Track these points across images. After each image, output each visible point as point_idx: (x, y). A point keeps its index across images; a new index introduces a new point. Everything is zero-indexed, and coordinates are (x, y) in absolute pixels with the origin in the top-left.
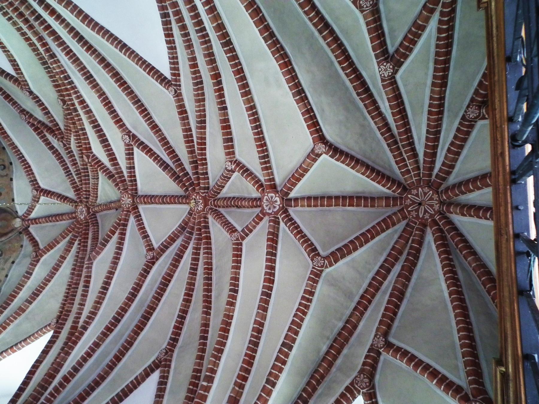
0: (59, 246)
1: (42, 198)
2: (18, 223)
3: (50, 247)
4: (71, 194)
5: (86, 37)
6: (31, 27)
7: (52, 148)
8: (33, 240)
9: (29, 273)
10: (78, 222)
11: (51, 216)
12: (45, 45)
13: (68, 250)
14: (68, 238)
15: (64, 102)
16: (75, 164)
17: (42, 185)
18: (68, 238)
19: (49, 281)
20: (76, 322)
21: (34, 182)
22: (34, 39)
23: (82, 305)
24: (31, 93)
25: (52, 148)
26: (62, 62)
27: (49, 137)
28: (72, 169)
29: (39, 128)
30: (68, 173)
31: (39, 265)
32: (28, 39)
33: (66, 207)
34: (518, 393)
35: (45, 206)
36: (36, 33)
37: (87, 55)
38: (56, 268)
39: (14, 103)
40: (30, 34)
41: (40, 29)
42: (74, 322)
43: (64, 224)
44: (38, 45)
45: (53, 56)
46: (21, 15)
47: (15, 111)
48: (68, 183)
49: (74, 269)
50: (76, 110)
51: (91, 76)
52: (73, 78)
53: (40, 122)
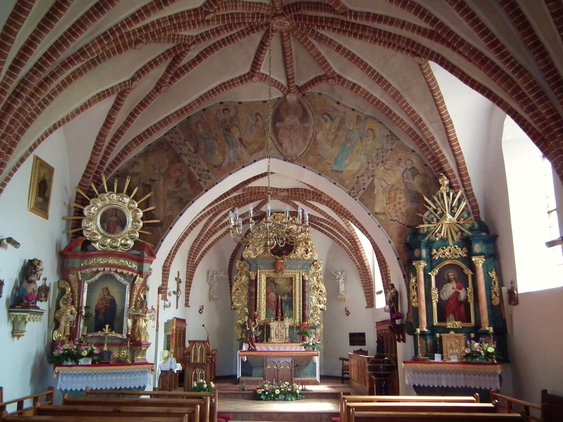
0: (323, 53)
1: (262, 71)
3: (323, 63)
4: (257, 37)
8: (312, 83)
9: (354, 87)
10: (294, 29)
12: (70, 61)
15: (137, 42)
16: (217, 31)
17: (247, 70)
18: (315, 42)
21: (243, 79)
22: (68, 73)
23: (403, 24)
24: (133, 79)
26: (87, 41)
27: (185, 61)
28: (225, 35)
29: (175, 72)
31: (344, 76)
33: (274, 42)
35: (272, 66)
38: (352, 57)
40: (62, 77)
43: (295, 47)
46: (41, 85)
47: (158, 97)
48: (243, 40)
50: (146, 27)
53: (168, 71)
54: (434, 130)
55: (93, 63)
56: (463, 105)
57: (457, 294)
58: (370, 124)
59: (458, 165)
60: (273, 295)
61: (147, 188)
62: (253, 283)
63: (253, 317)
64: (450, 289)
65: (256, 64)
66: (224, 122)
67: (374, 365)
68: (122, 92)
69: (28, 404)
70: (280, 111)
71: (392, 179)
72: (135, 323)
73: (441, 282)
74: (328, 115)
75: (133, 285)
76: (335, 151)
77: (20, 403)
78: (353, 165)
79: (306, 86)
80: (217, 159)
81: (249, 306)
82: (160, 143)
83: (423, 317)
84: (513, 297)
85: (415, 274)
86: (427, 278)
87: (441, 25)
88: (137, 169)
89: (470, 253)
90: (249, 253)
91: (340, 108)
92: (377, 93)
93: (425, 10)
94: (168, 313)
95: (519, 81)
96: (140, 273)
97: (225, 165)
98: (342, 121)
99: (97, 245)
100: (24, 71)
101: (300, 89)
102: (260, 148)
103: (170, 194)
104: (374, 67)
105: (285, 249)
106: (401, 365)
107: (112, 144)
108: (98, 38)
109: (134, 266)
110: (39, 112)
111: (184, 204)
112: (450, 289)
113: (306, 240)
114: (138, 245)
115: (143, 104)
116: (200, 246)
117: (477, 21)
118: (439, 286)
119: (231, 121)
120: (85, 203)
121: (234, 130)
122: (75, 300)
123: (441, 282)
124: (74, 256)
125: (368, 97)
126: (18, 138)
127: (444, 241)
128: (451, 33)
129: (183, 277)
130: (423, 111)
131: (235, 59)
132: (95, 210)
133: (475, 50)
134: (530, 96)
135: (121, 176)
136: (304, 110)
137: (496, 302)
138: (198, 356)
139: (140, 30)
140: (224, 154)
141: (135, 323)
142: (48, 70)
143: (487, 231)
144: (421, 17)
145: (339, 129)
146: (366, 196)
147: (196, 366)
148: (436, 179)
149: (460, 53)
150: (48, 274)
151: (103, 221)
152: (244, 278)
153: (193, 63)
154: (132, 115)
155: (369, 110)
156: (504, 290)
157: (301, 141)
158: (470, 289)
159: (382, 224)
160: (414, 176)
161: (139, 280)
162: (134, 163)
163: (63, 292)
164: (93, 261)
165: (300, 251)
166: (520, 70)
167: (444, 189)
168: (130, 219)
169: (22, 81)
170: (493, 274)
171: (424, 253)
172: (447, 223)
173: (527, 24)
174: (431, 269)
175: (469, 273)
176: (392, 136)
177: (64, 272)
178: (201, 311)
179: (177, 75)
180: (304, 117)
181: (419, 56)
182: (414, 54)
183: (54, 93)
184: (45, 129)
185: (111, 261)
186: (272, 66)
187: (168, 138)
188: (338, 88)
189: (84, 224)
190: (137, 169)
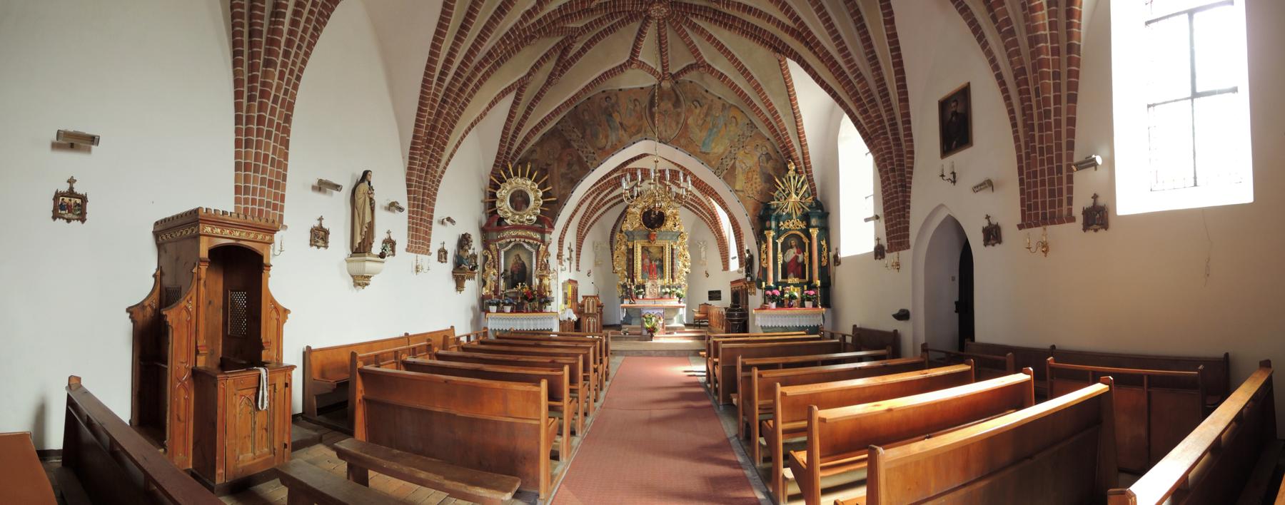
0: (695, 42)
1: (640, 58)
2: (666, 85)
3: (695, 52)
4: (635, 26)
5: (463, 15)
6: (469, 79)
7: (584, 50)
8: (685, 71)
9: (721, 76)
10: (670, 17)
11: (661, 48)
12: (481, 64)
13: (702, 32)
14: (688, 31)
15: (532, 37)
16: (600, 21)
17: (626, 58)
18: (688, 31)
19: (733, 56)
20: (786, 29)
21: (622, 68)
22: (479, 75)
23: (769, 18)
24: (529, 74)
25: (584, 50)
26: (493, 43)
27: (571, 54)
28: (607, 25)
29: (563, 65)
30: (611, 29)
31: (713, 65)
32: (480, 82)
33: (651, 32)
34: (180, 222)
35: (648, 54)
36: (473, 75)
37: (478, 16)
38: (721, 47)
39: (542, 91)
40: (475, 81)
41: (468, 72)
42: (787, 31)
43: (670, 34)
44: (484, 71)
45: (489, 54)
46: (461, 90)
47: (550, 91)
48: (623, 30)
49: (726, 25)
50: (539, 21)
51: (499, 8)
52: (507, 29)
53: (557, 64)
54: (787, 122)
55: (498, 64)
56: (811, 99)
57: (797, 257)
58: (733, 113)
59: (803, 154)
60: (647, 261)
61: (544, 172)
62: (631, 252)
63: (631, 276)
64: (792, 253)
65: (635, 52)
66: (607, 108)
67: (730, 312)
68: (520, 87)
69: (472, 339)
70: (653, 98)
71: (750, 161)
72: (541, 281)
73: (785, 247)
74: (697, 101)
75: (538, 252)
76: (704, 134)
77: (468, 337)
78: (718, 148)
79: (678, 74)
80: (602, 141)
81: (628, 270)
82: (553, 132)
83: (771, 275)
84: (837, 261)
85: (766, 241)
86: (775, 244)
87: (802, 24)
88: (535, 156)
89: (809, 226)
90: (627, 226)
91: (710, 97)
92: (741, 83)
93: (790, 8)
94: (564, 276)
95: (858, 87)
96: (543, 241)
97: (608, 147)
98: (710, 108)
99: (508, 221)
100: (448, 79)
101: (673, 77)
102: (638, 132)
103: (563, 176)
104: (740, 59)
105: (654, 220)
106: (752, 311)
107: (514, 137)
108: (502, 39)
109: (538, 236)
110: (460, 114)
111: (574, 182)
112: (792, 253)
113: (675, 215)
114: (539, 220)
115: (538, 98)
116: (587, 221)
117: (832, 25)
118: (784, 251)
119: (613, 106)
120: (497, 187)
121: (615, 115)
122: (496, 265)
123: (785, 247)
124: (493, 230)
125: (733, 86)
126: (447, 138)
127: (789, 216)
128: (810, 33)
129: (574, 247)
130: (779, 104)
131: (615, 49)
132: (504, 193)
133: (828, 52)
134: (865, 101)
135: (523, 163)
136: (677, 96)
137: (824, 263)
138: (590, 308)
139: (534, 25)
140: (607, 137)
141: (541, 281)
142: (465, 76)
143: (822, 209)
144: (786, 13)
145: (707, 115)
146: (728, 175)
147: (588, 315)
148: (785, 165)
149: (815, 53)
150: (476, 247)
151: (511, 201)
152: (623, 247)
153: (579, 54)
154: (529, 109)
155: (732, 99)
156: (831, 254)
157: (674, 124)
158: (807, 254)
159: (742, 200)
160: (768, 160)
161: (542, 247)
162: (532, 151)
163: (486, 258)
164: (506, 234)
165: (669, 224)
166: (859, 76)
167: (791, 173)
168: (532, 198)
169: (447, 89)
170: (823, 243)
171: (773, 224)
172: (792, 201)
173: (868, 39)
174: (779, 237)
175: (806, 241)
176: (751, 125)
177: (486, 244)
178: (589, 274)
179: (565, 68)
180: (677, 103)
181: (779, 52)
182: (776, 50)
183: (471, 96)
184: (465, 128)
185: (520, 233)
186: (648, 54)
187: (559, 127)
188: (708, 77)
189: (498, 204)
190: (535, 156)
